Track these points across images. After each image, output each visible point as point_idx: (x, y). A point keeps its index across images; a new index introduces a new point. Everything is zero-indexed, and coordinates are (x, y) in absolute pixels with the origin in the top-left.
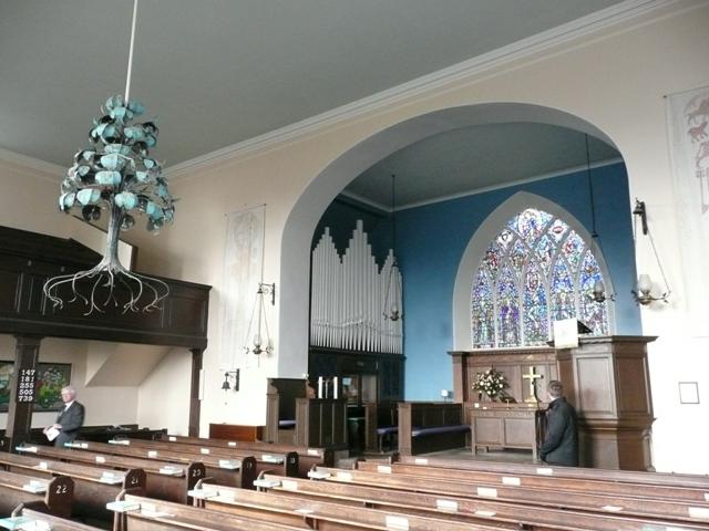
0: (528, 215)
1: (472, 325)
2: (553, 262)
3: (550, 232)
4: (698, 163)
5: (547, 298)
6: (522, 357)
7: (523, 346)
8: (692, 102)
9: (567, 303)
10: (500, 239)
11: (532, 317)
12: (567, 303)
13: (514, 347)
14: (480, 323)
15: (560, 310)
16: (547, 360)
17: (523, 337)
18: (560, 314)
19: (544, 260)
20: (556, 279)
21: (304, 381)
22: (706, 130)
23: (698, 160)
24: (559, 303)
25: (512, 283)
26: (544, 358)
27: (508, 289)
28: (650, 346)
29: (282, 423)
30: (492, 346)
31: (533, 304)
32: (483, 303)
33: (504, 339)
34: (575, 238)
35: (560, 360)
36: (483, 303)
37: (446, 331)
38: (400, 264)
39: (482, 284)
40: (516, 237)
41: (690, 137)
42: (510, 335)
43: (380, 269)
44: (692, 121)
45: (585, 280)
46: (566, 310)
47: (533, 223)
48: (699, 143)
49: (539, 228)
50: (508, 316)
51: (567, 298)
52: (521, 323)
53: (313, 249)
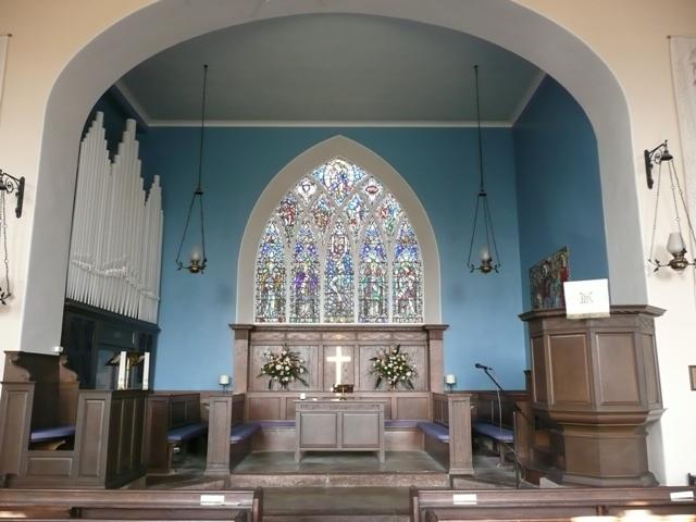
0: (337, 167)
1: (256, 293)
2: (365, 227)
3: (363, 191)
5: (355, 268)
6: (325, 336)
7: (322, 322)
9: (377, 274)
10: (300, 190)
11: (334, 288)
12: (377, 274)
13: (310, 323)
14: (266, 290)
15: (369, 282)
16: (356, 340)
17: (322, 311)
18: (369, 287)
19: (354, 222)
20: (367, 245)
21: (53, 359)
25: (312, 244)
26: (283, 335)
27: (305, 253)
29: (36, 436)
30: (280, 320)
31: (336, 272)
32: (271, 266)
33: (366, 311)
34: (394, 204)
35: (534, 338)
36: (271, 266)
37: (226, 296)
38: (165, 204)
39: (272, 241)
40: (320, 190)
42: (305, 308)
43: (147, 197)
45: (399, 251)
46: (375, 283)
47: (343, 177)
49: (350, 184)
50: (304, 285)
51: (378, 269)
52: (322, 295)
53: (82, 140)
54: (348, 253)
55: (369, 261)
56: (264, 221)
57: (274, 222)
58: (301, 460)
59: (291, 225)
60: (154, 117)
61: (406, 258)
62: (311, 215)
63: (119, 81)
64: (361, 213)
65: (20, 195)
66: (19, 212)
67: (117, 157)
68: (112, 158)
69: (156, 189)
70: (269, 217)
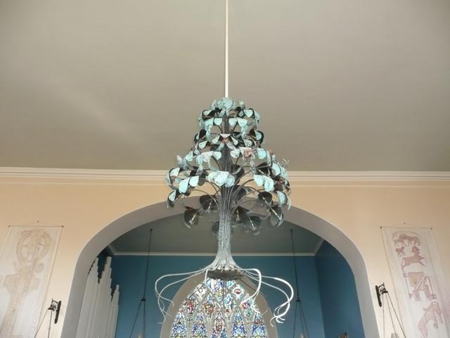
3: (233, 292)
20: (235, 326)
27: (199, 329)
38: (120, 303)
39: (180, 323)
45: (254, 329)
54: (224, 331)
55: (237, 335)
56: (176, 310)
57: (182, 311)
58: (190, 224)
59: (191, 313)
60: (118, 250)
61: (258, 334)
62: (203, 306)
63: (111, 244)
64: (232, 305)
65: (58, 312)
66: (56, 321)
67: (101, 280)
68: (99, 282)
69: (117, 292)
70: (178, 308)
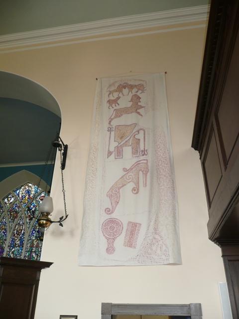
4: (110, 122)
5: (25, 242)
8: (113, 84)
22: (119, 102)
23: (114, 195)
24: (32, 246)
28: (44, 273)
41: (108, 105)
44: (111, 95)
46: (35, 252)
47: (28, 192)
48: (113, 109)
49: (32, 195)
